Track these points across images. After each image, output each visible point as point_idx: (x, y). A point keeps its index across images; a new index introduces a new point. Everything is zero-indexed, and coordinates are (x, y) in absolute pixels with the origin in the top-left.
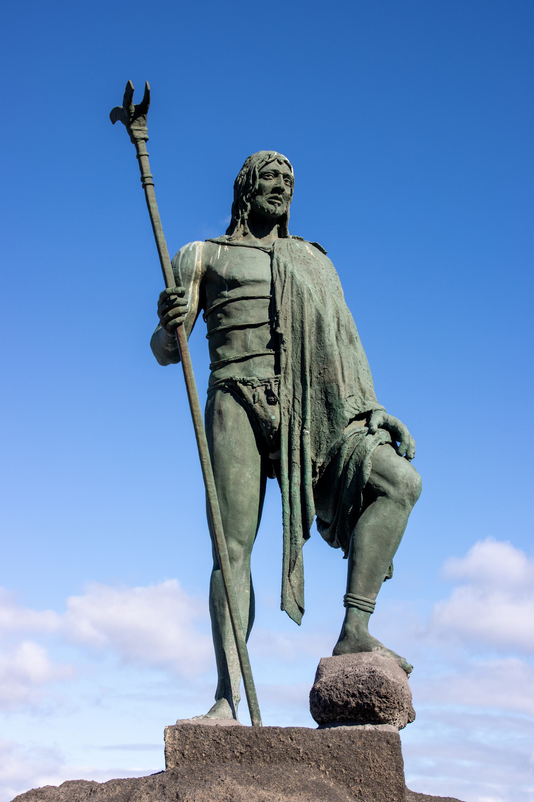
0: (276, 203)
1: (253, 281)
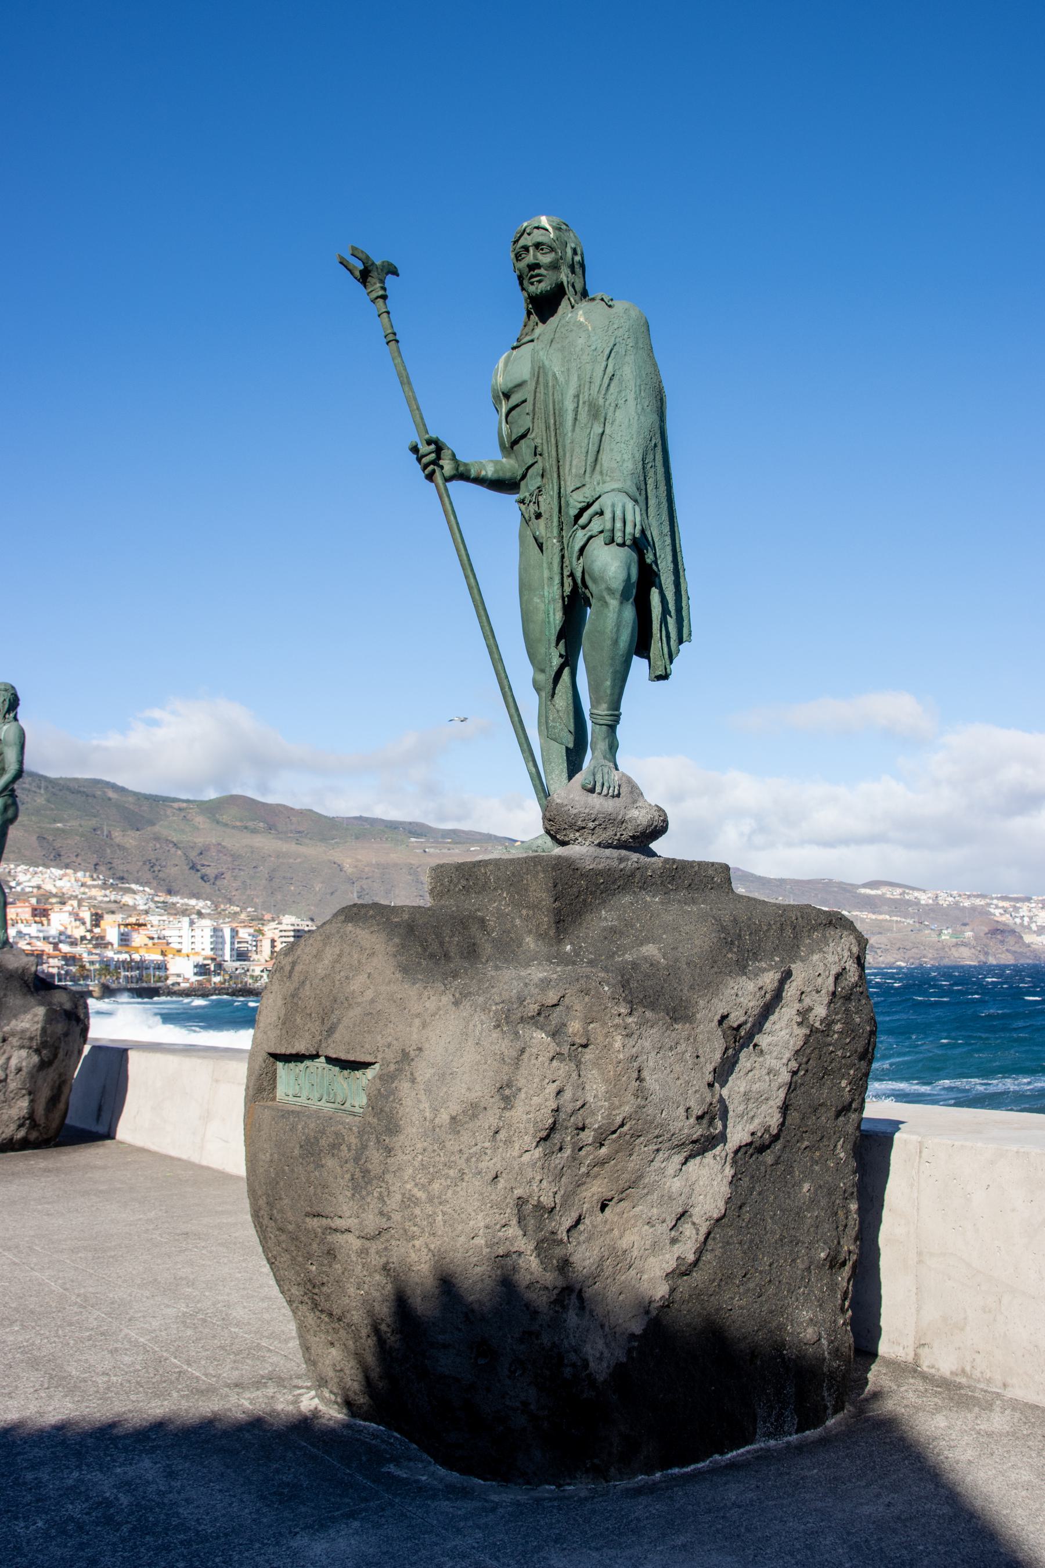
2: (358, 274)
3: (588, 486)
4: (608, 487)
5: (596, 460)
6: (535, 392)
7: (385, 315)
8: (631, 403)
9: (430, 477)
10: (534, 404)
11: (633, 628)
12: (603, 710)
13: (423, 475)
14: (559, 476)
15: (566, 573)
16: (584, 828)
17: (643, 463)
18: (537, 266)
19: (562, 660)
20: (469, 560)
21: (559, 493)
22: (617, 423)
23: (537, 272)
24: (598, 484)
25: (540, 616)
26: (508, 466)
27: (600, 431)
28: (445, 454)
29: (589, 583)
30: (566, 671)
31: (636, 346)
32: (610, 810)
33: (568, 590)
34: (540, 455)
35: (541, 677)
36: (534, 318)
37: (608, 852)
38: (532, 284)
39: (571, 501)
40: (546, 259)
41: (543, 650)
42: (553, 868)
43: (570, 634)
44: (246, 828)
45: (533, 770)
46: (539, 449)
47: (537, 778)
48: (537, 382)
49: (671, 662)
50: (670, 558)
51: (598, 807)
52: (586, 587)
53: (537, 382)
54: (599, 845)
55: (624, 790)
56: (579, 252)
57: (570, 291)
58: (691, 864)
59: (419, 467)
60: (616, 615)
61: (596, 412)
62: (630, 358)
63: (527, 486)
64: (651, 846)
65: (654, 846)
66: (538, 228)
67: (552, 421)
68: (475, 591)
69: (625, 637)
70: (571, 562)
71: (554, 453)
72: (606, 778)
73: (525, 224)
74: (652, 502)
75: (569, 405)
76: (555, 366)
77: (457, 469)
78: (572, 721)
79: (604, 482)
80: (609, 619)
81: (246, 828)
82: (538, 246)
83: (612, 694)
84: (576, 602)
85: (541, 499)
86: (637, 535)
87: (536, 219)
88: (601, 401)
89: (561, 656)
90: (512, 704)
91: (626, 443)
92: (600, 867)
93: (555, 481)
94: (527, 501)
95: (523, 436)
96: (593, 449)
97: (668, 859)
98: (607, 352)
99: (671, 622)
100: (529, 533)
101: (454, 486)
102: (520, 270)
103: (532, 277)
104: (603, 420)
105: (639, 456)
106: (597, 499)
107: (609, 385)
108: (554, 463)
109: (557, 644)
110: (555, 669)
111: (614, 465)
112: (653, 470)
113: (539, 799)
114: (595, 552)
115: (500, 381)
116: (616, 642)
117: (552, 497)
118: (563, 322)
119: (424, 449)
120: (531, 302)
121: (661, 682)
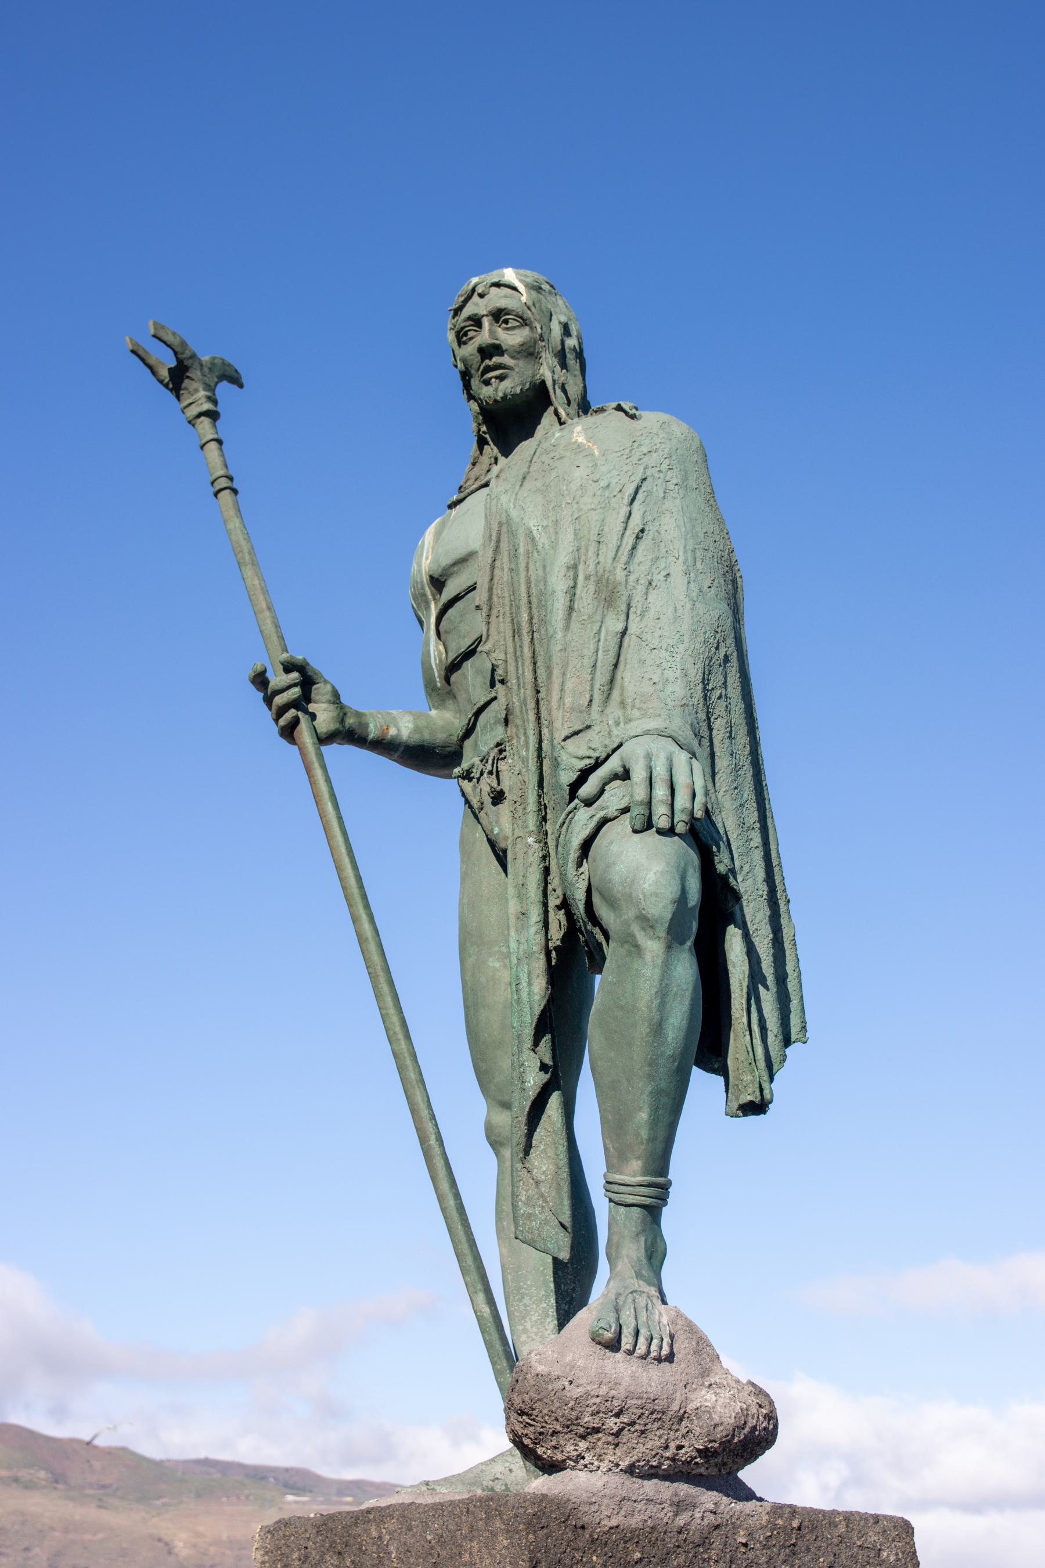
0: (491, 379)
1: (454, 564)
2: (164, 373)
3: (596, 728)
4: (636, 727)
5: (612, 681)
6: (493, 568)
7: (213, 445)
8: (679, 579)
9: (289, 732)
10: (490, 590)
11: (693, 1001)
12: (633, 1172)
13: (275, 730)
14: (538, 718)
15: (554, 901)
16: (597, 1430)
17: (705, 689)
18: (496, 349)
19: (545, 1077)
20: (361, 887)
21: (540, 749)
22: (651, 614)
23: (496, 360)
24: (617, 724)
25: (502, 994)
26: (440, 723)
27: (620, 627)
28: (321, 692)
29: (602, 910)
30: (555, 1100)
31: (683, 484)
32: (654, 1389)
33: (556, 935)
34: (502, 682)
35: (503, 1118)
36: (491, 450)
37: (650, 1487)
38: (487, 383)
39: (564, 757)
40: (512, 338)
41: (505, 1063)
42: (529, 1524)
43: (561, 1022)
44: (16, 1480)
45: (486, 1310)
46: (500, 672)
47: (493, 1330)
48: (497, 549)
49: (771, 1079)
50: (760, 873)
51: (626, 1382)
52: (595, 921)
53: (497, 549)
54: (630, 1470)
55: (682, 1348)
56: (574, 333)
57: (557, 398)
58: (829, 1518)
59: (268, 715)
60: (658, 971)
61: (609, 594)
62: (674, 504)
63: (476, 745)
64: (742, 1475)
65: (748, 1475)
66: (497, 285)
67: (525, 617)
68: (372, 947)
69: (680, 1017)
70: (563, 876)
71: (529, 676)
72: (643, 1318)
73: (475, 280)
74: (723, 763)
75: (559, 584)
76: (530, 515)
77: (342, 721)
78: (567, 1202)
79: (628, 720)
80: (644, 984)
81: (16, 1480)
82: (498, 315)
83: (652, 1140)
84: (575, 956)
85: (502, 766)
86: (699, 814)
87: (495, 273)
88: (620, 575)
89: (544, 1067)
90: (442, 1173)
91: (671, 650)
92: (634, 1522)
93: (531, 726)
94: (476, 774)
95: (469, 654)
96: (605, 661)
97: (782, 1507)
98: (630, 490)
99: (768, 998)
100: (480, 835)
101: (338, 754)
102: (464, 361)
103: (488, 369)
104: (624, 607)
105: (695, 674)
106: (614, 750)
107: (634, 548)
108: (529, 692)
109: (536, 1043)
110: (532, 1094)
111: (647, 688)
112: (722, 703)
113: (498, 1374)
114: (614, 848)
115: (427, 558)
116: (658, 1029)
117: (524, 760)
118: (545, 445)
119: (278, 679)
120: (485, 422)
121: (752, 1119)
